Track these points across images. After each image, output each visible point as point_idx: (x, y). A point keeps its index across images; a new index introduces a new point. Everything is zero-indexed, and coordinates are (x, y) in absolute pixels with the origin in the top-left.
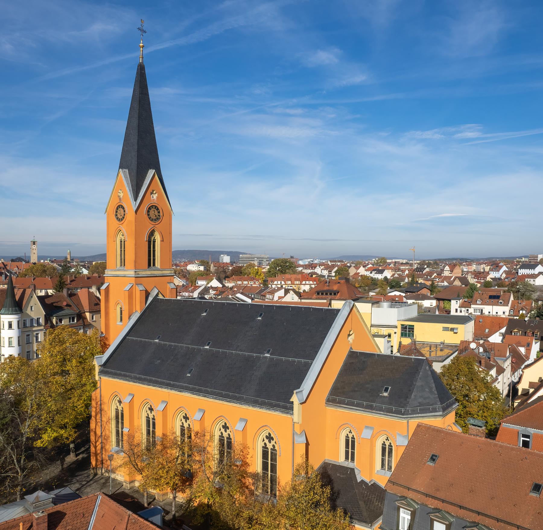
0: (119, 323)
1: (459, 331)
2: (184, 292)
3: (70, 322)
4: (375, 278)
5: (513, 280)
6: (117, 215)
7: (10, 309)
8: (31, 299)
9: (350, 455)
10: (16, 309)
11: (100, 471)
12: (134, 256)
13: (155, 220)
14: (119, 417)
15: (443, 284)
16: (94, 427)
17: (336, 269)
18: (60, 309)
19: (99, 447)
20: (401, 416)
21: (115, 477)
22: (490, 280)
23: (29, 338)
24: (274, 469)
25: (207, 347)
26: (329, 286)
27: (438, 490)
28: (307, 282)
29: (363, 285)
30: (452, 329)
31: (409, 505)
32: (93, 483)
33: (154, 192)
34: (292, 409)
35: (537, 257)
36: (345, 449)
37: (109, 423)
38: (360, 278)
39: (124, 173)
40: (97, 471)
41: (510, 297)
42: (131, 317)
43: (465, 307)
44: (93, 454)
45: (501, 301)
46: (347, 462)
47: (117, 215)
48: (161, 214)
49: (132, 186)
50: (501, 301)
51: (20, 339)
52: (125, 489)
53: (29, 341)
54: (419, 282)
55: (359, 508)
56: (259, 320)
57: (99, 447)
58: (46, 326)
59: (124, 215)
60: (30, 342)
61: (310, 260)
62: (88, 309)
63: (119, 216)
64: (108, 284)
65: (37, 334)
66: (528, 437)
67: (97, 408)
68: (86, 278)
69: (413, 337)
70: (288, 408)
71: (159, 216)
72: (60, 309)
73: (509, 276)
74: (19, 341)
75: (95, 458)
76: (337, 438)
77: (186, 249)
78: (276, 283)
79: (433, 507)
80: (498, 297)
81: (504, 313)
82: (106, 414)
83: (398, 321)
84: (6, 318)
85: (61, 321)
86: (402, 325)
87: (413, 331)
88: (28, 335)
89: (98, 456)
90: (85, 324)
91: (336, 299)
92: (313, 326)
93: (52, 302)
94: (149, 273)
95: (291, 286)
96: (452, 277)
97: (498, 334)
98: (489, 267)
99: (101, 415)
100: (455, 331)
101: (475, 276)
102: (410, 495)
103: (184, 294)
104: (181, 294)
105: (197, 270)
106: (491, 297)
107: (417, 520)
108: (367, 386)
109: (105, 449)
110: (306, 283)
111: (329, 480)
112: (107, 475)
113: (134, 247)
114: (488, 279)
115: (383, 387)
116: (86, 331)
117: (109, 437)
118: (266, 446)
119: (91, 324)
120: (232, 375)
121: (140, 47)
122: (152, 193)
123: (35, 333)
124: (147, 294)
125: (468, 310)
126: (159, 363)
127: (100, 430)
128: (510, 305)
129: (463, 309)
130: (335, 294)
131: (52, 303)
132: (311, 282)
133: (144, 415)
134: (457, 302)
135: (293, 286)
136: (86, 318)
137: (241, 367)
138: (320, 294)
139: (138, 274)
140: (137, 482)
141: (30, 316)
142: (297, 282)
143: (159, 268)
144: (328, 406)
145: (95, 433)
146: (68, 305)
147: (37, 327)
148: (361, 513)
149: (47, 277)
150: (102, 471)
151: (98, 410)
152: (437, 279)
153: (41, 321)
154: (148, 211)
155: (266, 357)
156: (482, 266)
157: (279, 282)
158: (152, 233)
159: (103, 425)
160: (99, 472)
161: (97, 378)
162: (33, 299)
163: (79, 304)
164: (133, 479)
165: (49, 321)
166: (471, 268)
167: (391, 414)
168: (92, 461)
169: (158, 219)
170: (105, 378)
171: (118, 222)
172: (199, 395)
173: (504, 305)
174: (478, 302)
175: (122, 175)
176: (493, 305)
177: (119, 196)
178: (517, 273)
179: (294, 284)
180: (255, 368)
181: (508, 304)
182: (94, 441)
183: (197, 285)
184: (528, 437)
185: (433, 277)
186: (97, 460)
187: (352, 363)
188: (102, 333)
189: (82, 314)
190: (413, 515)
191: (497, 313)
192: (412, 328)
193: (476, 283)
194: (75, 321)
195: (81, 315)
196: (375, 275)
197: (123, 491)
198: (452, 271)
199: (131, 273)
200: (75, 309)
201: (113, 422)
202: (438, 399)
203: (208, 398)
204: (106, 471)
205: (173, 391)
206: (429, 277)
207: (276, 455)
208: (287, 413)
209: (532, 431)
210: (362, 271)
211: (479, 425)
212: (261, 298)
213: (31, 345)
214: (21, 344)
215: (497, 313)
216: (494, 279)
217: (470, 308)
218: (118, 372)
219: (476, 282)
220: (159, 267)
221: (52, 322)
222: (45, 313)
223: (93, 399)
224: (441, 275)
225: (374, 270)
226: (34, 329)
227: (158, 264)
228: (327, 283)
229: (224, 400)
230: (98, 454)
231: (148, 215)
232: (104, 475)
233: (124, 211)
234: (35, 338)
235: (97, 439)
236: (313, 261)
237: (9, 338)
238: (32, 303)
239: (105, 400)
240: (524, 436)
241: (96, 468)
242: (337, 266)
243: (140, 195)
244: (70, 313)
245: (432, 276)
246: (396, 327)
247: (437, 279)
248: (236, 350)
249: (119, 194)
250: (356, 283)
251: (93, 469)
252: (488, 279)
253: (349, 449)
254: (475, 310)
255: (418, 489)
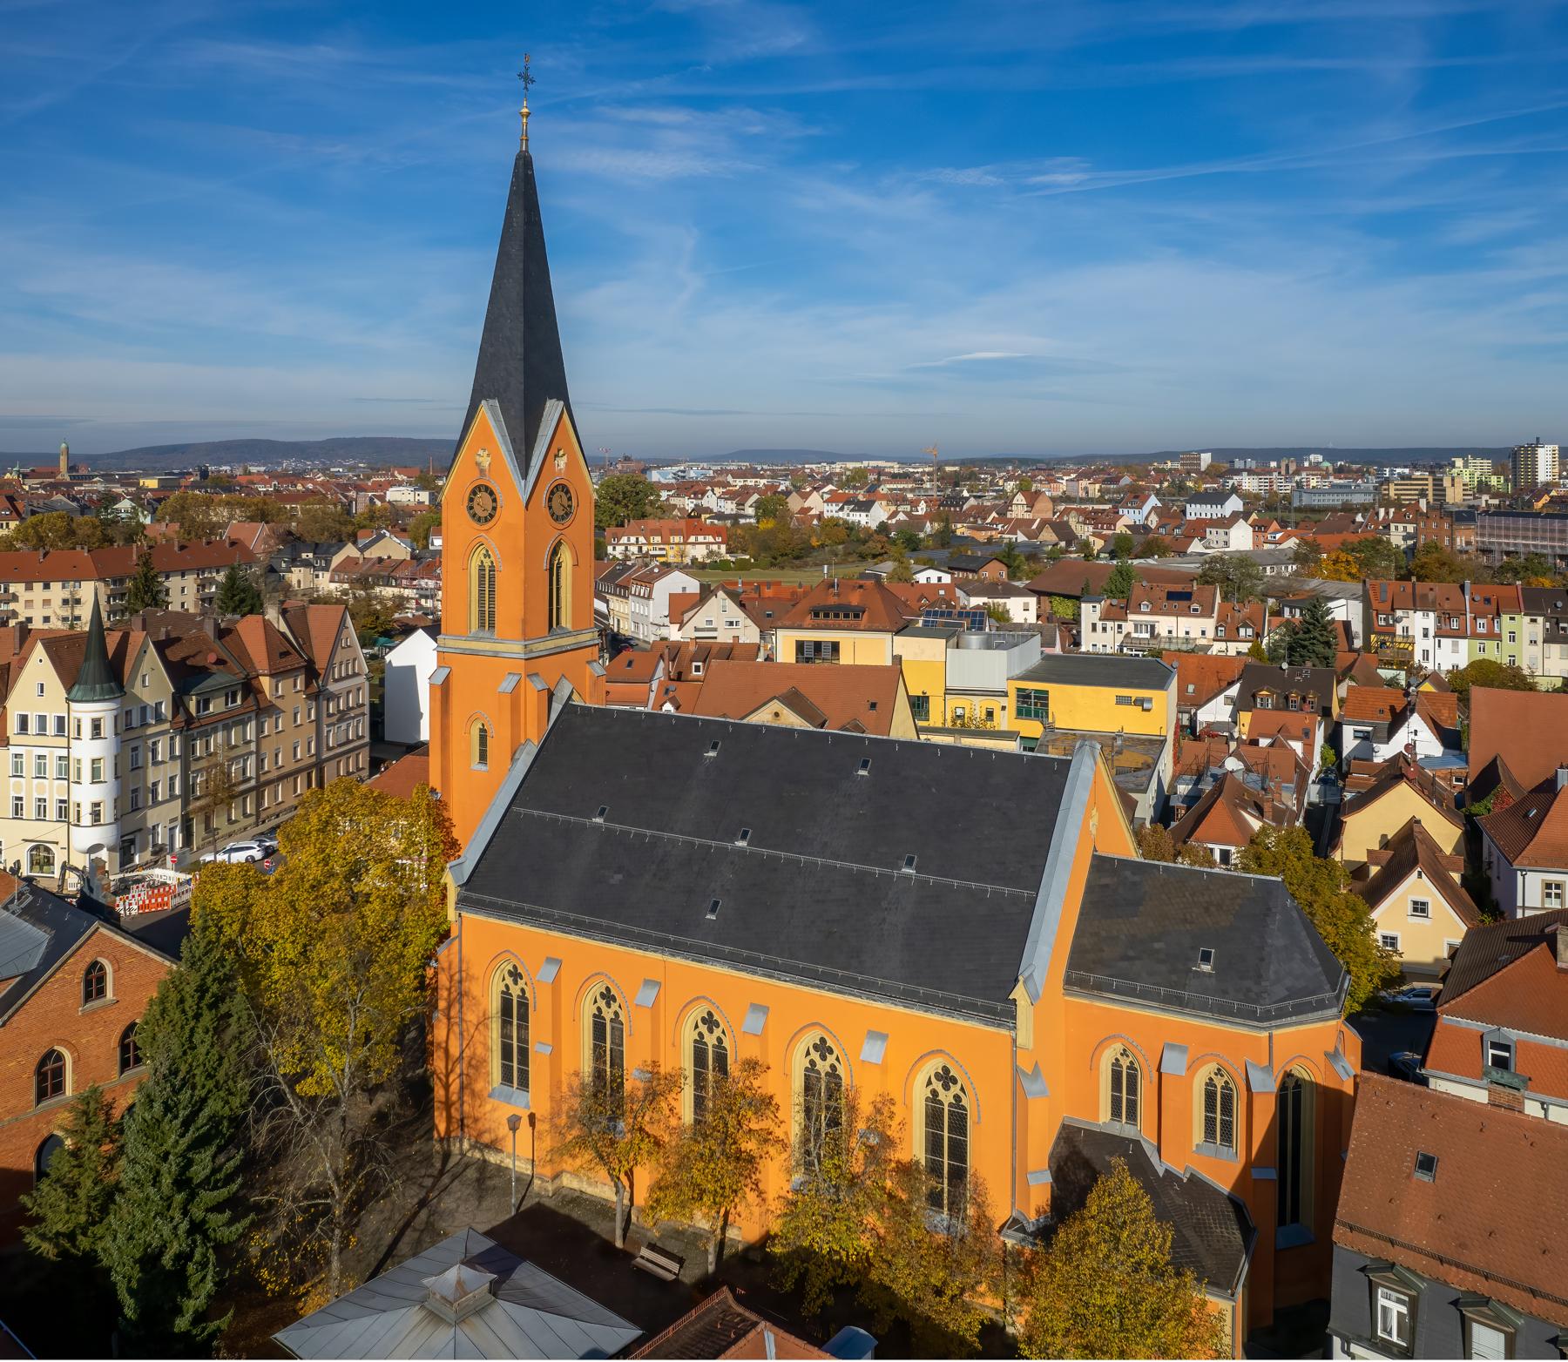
1: (1154, 705)
2: (423, 578)
3: (227, 704)
5: (1177, 531)
6: (471, 508)
7: (97, 686)
8: (143, 656)
10: (111, 688)
11: (458, 1145)
14: (514, 1011)
15: (1014, 537)
16: (445, 1038)
17: (755, 497)
18: (203, 673)
19: (455, 1087)
20: (1256, 1023)
21: (501, 1162)
22: (1124, 530)
24: (959, 1151)
25: (741, 844)
26: (838, 595)
27: (1462, 1246)
28: (701, 539)
29: (829, 542)
30: (1139, 702)
31: (1404, 1283)
32: (452, 1181)
33: (561, 453)
34: (1013, 1016)
36: (1110, 1093)
37: (486, 1027)
40: (449, 1146)
41: (1215, 594)
42: (517, 756)
43: (1114, 620)
44: (439, 1105)
47: (471, 508)
48: (574, 504)
49: (513, 441)
50: (1195, 606)
52: (539, 1195)
54: (958, 533)
56: (863, 776)
57: (455, 1087)
58: (176, 720)
59: (494, 509)
60: (140, 765)
64: (447, 671)
65: (155, 744)
66: (1506, 1048)
67: (453, 989)
68: (176, 548)
69: (1047, 717)
70: (1004, 1013)
71: (570, 506)
72: (203, 673)
73: (1167, 521)
74: (116, 764)
75: (444, 1114)
76: (1093, 1066)
78: (626, 542)
79: (1463, 1289)
80: (1186, 596)
81: (1203, 633)
82: (475, 1005)
83: (1008, 679)
87: (1047, 705)
88: (135, 749)
89: (453, 1110)
90: (262, 706)
91: (862, 628)
94: (551, 644)
95: (664, 549)
97: (1221, 698)
100: (1146, 705)
101: (1086, 518)
102: (1400, 1256)
103: (423, 583)
104: (415, 583)
105: (412, 500)
107: (1423, 1316)
108: (1157, 945)
110: (697, 539)
112: (478, 1155)
114: (1120, 527)
115: (1194, 948)
116: (263, 723)
117: (485, 1061)
118: (937, 1096)
119: (274, 705)
121: (523, 116)
122: (556, 456)
123: (150, 742)
125: (1120, 627)
126: (620, 881)
127: (458, 1044)
128: (1215, 615)
129: (1109, 624)
132: (710, 539)
133: (588, 1011)
134: (1094, 607)
135: (666, 547)
136: (261, 691)
138: (821, 615)
139: (531, 651)
140: (569, 1175)
141: (141, 700)
142: (677, 539)
143: (571, 629)
144: (1068, 995)
145: (447, 1051)
146: (220, 662)
147: (155, 725)
148: (1199, 1262)
149: (78, 548)
150: (461, 1145)
151: (454, 994)
153: (163, 710)
154: (550, 500)
155: (907, 878)
157: (633, 540)
159: (468, 1030)
160: (455, 1149)
161: (452, 914)
163: (243, 657)
164: (558, 1169)
165: (181, 709)
166: (1057, 489)
167: (1231, 1019)
168: (437, 1121)
172: (754, 973)
173: (1202, 616)
177: (478, 464)
180: (884, 904)
181: (1213, 612)
182: (444, 1071)
183: (431, 548)
184: (1506, 1048)
185: (989, 520)
186: (449, 1119)
187: (1107, 886)
189: (253, 682)
190: (1413, 1305)
191: (1187, 633)
192: (1043, 697)
194: (239, 702)
195: (251, 685)
196: (851, 514)
197: (539, 1203)
199: (516, 648)
201: (494, 1026)
202: (1324, 978)
203: (779, 979)
204: (473, 1147)
205: (678, 958)
209: (1513, 1035)
211: (1514, 1085)
212: (615, 590)
213: (141, 771)
215: (1187, 633)
216: (1133, 528)
217: (1126, 620)
218: (514, 904)
219: (1094, 534)
221: (187, 711)
222: (174, 687)
223: (443, 969)
224: (1005, 514)
226: (150, 731)
227: (566, 622)
228: (833, 586)
229: (823, 988)
230: (454, 1103)
231: (550, 508)
232: (469, 1154)
233: (494, 500)
234: (150, 754)
235: (450, 1067)
237: (94, 761)
238: (145, 668)
240: (1495, 1046)
242: (756, 489)
243: (533, 463)
244: (227, 682)
245: (985, 519)
246: (1005, 694)
248: (821, 854)
249: (479, 459)
251: (441, 1140)
252: (1120, 527)
253: (1121, 1092)
254: (1136, 626)
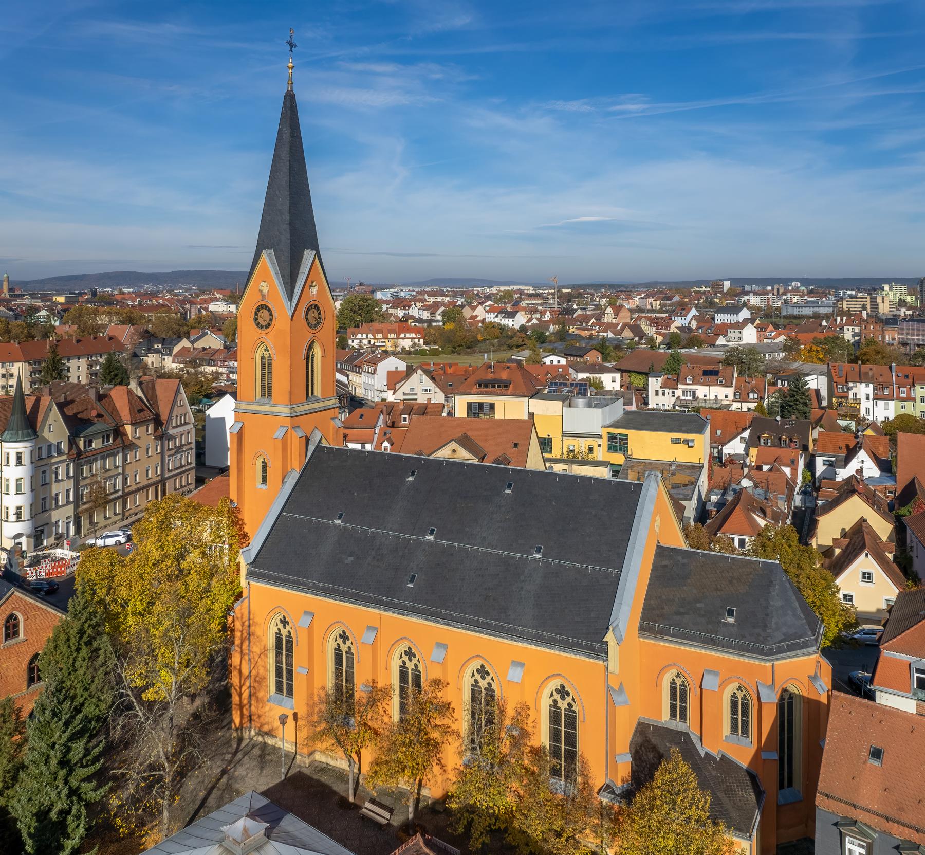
0: (259, 485)
1: (696, 444)
3: (103, 443)
4: (504, 325)
5: (709, 331)
7: (20, 432)
9: (679, 709)
11: (248, 733)
12: (288, 383)
13: (315, 326)
15: (606, 334)
16: (239, 663)
17: (442, 309)
18: (87, 423)
19: (245, 695)
20: (763, 657)
23: (45, 476)
24: (571, 740)
26: (493, 373)
27: (901, 809)
28: (408, 335)
30: (686, 442)
31: (863, 834)
32: (243, 757)
33: (314, 284)
35: (723, 285)
37: (266, 656)
38: (480, 325)
39: (269, 255)
40: (242, 733)
41: (733, 372)
42: (286, 480)
45: (721, 379)
46: (674, 722)
48: (323, 316)
49: (283, 276)
51: (34, 479)
52: (300, 766)
53: (45, 481)
55: (720, 804)
56: (508, 494)
57: (245, 695)
59: (271, 320)
60: (47, 482)
61: (393, 290)
62: (129, 419)
63: (260, 321)
65: (57, 468)
67: (244, 632)
68: (74, 342)
70: (599, 650)
71: (320, 318)
72: (87, 423)
73: (702, 324)
75: (239, 712)
77: (192, 269)
80: (715, 373)
81: (726, 396)
82: (258, 641)
84: (12, 448)
85: (90, 442)
86: (609, 434)
88: (44, 472)
89: (244, 710)
92: (602, 509)
93: (75, 411)
94: (308, 407)
96: (618, 324)
97: (738, 439)
98: (658, 302)
99: (250, 643)
100: (690, 444)
101: (652, 323)
102: (861, 816)
104: (226, 363)
106: (706, 373)
108: (698, 605)
109: (257, 698)
111: (656, 755)
112: (260, 739)
113: (288, 370)
114: (673, 328)
120: (486, 589)
122: (311, 286)
123: (54, 467)
124: (308, 440)
125: (673, 392)
127: (247, 667)
129: (667, 391)
130: (505, 386)
131: (76, 414)
135: (386, 341)
136: (126, 435)
137: (498, 575)
138: (483, 385)
141: (48, 441)
142: (393, 336)
144: (642, 637)
146: (99, 416)
147: (57, 457)
149: (12, 341)
151: (245, 635)
152: (597, 328)
154: (307, 314)
156: (650, 300)
157: (365, 336)
158: (310, 347)
160: (246, 735)
161: (243, 583)
162: (52, 413)
163: (114, 412)
166: (633, 304)
168: (234, 717)
169: (318, 323)
170: (255, 584)
171: (259, 330)
172: (438, 622)
174: (688, 381)
175: (267, 260)
176: (710, 385)
177: (260, 291)
178: (713, 319)
179: (387, 338)
180: (522, 578)
181: (732, 383)
185: (590, 324)
188: (232, 501)
191: (716, 396)
192: (625, 438)
193: (655, 336)
194: (111, 441)
198: (616, 314)
199: (285, 410)
200: (110, 420)
204: (257, 734)
206: (584, 325)
207: (574, 718)
208: (597, 658)
210: (481, 313)
213: (47, 486)
214: (34, 488)
215: (716, 396)
218: (283, 576)
219: (656, 333)
220: (320, 396)
221: (78, 447)
223: (238, 618)
224: (600, 320)
225: (501, 312)
226: (54, 460)
227: (318, 392)
228: (490, 367)
229: (483, 633)
230: (245, 706)
231: (307, 319)
232: (255, 739)
233: (271, 315)
234: (54, 475)
235: (242, 682)
236: (397, 292)
237: (17, 480)
238: (50, 420)
239: (259, 618)
241: (240, 728)
242: (442, 304)
243: (296, 291)
245: (588, 323)
247: (597, 328)
249: (261, 288)
250: (477, 334)
254: (683, 392)
255: (870, 807)
